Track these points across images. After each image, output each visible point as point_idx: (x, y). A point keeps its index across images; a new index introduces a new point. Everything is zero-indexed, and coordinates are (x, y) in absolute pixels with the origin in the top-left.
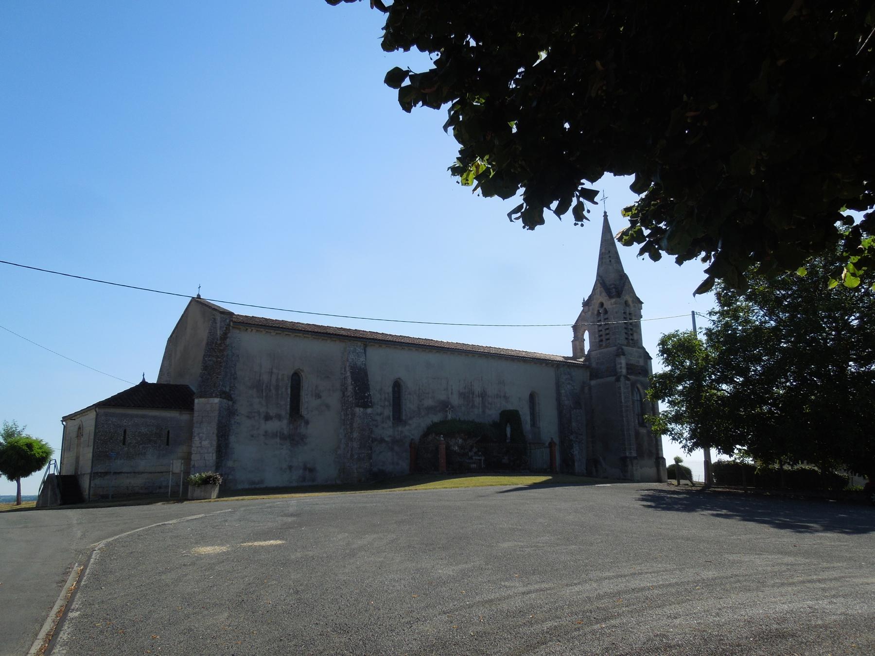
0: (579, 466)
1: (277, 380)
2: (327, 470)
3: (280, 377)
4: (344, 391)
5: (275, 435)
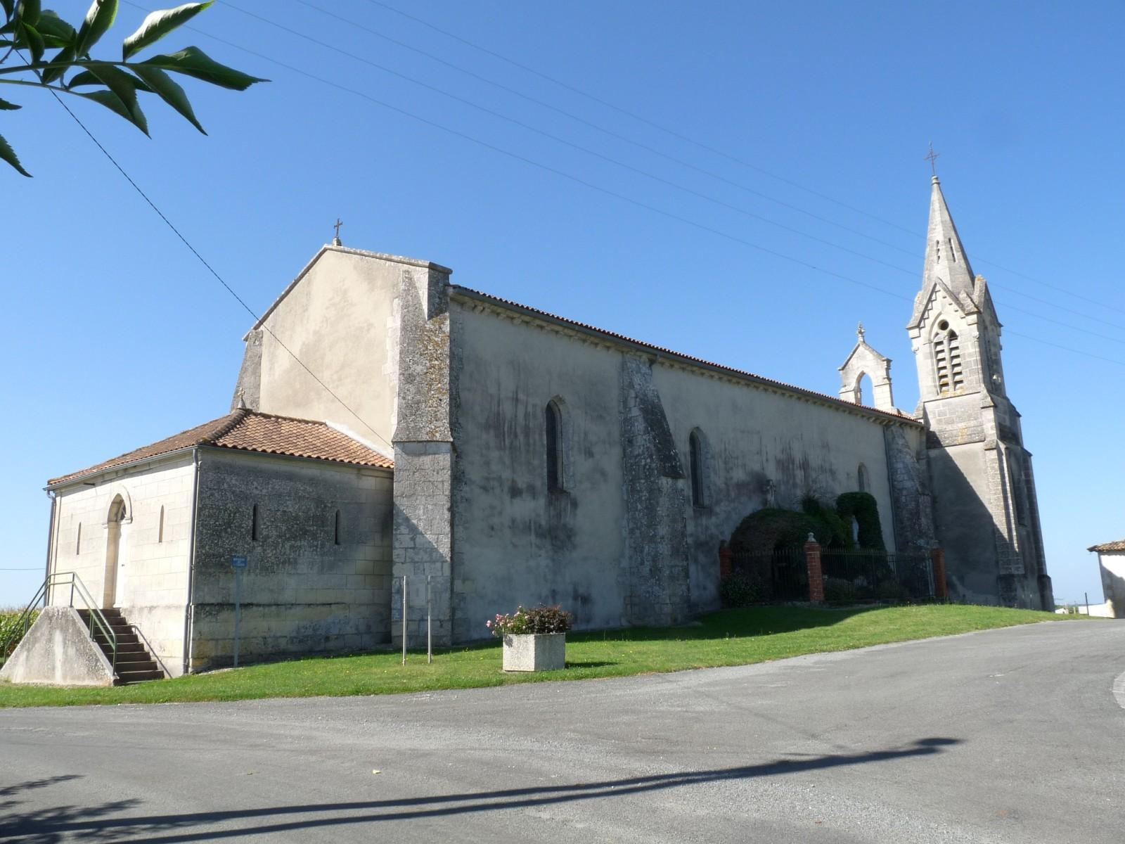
0: (424, 647)
1: (526, 415)
2: (608, 604)
3: (530, 409)
4: (628, 441)
5: (527, 528)
